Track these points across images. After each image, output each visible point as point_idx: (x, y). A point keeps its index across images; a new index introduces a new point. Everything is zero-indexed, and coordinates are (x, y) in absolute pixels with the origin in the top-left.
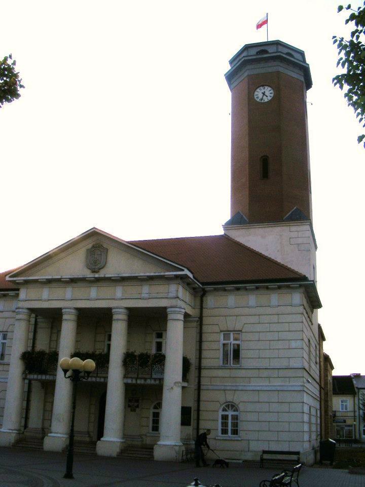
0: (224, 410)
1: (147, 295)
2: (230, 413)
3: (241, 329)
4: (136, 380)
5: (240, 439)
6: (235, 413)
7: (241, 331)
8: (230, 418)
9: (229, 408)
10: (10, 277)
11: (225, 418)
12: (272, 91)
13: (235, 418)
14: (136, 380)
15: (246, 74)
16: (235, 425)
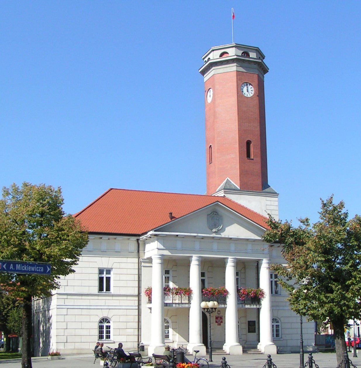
1: (251, 250)
2: (105, 325)
5: (282, 339)
6: (277, 324)
8: (105, 327)
9: (104, 321)
10: (155, 231)
11: (101, 327)
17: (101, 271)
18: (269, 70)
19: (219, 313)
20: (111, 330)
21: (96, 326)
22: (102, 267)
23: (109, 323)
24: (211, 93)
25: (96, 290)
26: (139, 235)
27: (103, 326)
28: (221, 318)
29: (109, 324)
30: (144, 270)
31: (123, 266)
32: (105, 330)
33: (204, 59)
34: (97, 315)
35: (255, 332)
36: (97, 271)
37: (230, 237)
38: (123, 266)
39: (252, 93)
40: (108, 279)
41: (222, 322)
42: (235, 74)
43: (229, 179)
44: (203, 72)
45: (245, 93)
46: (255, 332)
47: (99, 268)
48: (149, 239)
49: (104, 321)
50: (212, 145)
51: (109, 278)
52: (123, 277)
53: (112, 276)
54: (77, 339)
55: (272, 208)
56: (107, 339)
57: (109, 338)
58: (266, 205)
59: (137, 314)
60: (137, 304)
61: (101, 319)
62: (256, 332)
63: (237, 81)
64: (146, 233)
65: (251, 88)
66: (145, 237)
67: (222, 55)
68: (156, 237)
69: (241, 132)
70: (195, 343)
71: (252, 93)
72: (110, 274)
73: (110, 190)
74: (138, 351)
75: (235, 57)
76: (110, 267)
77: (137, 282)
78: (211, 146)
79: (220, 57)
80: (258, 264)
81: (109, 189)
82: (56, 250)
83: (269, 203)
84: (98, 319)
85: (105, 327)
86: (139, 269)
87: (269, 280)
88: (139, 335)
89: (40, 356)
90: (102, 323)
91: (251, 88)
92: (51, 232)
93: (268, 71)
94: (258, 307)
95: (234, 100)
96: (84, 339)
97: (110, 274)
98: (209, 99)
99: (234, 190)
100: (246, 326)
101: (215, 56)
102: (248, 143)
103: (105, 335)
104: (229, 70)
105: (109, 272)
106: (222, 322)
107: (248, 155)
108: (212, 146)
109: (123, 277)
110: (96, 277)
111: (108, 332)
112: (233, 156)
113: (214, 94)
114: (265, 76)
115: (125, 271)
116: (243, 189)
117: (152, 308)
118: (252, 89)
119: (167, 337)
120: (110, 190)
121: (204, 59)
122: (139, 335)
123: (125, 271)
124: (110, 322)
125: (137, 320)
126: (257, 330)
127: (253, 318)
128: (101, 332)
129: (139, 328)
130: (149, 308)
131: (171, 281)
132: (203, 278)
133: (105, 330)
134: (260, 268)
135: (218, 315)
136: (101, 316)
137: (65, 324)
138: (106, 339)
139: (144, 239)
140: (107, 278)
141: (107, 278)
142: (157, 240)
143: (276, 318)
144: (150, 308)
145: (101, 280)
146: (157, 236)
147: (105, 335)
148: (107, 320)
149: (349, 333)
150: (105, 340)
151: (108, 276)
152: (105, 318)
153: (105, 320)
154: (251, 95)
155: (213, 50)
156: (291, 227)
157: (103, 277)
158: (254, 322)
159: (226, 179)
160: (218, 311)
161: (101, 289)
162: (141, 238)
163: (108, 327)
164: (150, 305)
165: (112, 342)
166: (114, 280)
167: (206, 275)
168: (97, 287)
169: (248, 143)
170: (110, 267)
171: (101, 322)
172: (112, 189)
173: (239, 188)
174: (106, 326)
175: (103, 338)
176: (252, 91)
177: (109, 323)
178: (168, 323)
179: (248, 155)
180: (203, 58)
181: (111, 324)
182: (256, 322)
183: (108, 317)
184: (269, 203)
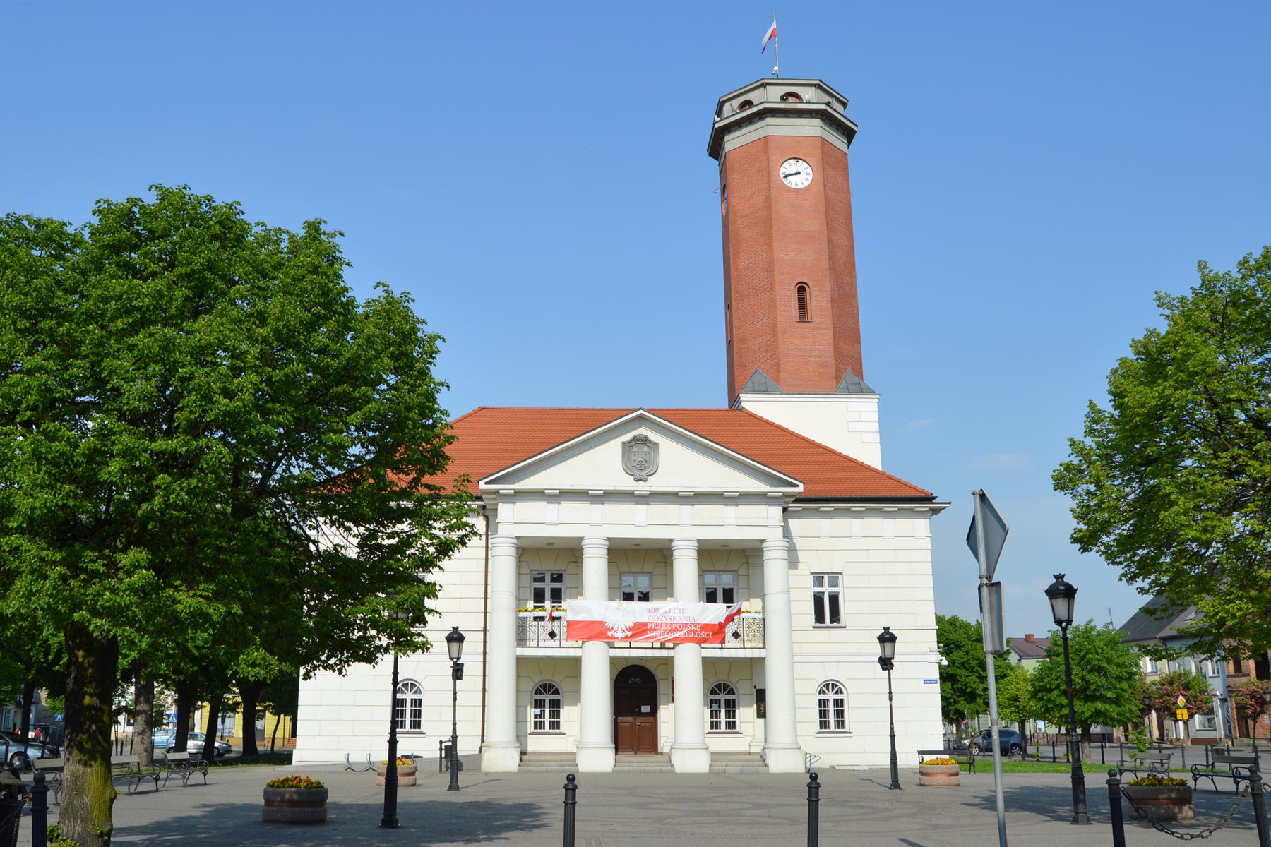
0: (821, 692)
2: (831, 696)
8: (831, 703)
9: (828, 689)
10: (486, 483)
11: (823, 703)
12: (810, 177)
13: (839, 703)
16: (840, 714)
32: (408, 709)
39: (807, 179)
49: (828, 689)
56: (552, 731)
67: (784, 98)
79: (717, 159)
82: (1240, 524)
85: (831, 703)
92: (28, 554)
103: (408, 719)
105: (834, 581)
132: (636, 597)
133: (408, 709)
136: (823, 679)
143: (842, 688)
145: (818, 600)
147: (408, 719)
148: (554, 686)
149: (116, 732)
151: (834, 590)
153: (830, 686)
156: (417, 489)
161: (819, 617)
174: (412, 700)
178: (841, 692)
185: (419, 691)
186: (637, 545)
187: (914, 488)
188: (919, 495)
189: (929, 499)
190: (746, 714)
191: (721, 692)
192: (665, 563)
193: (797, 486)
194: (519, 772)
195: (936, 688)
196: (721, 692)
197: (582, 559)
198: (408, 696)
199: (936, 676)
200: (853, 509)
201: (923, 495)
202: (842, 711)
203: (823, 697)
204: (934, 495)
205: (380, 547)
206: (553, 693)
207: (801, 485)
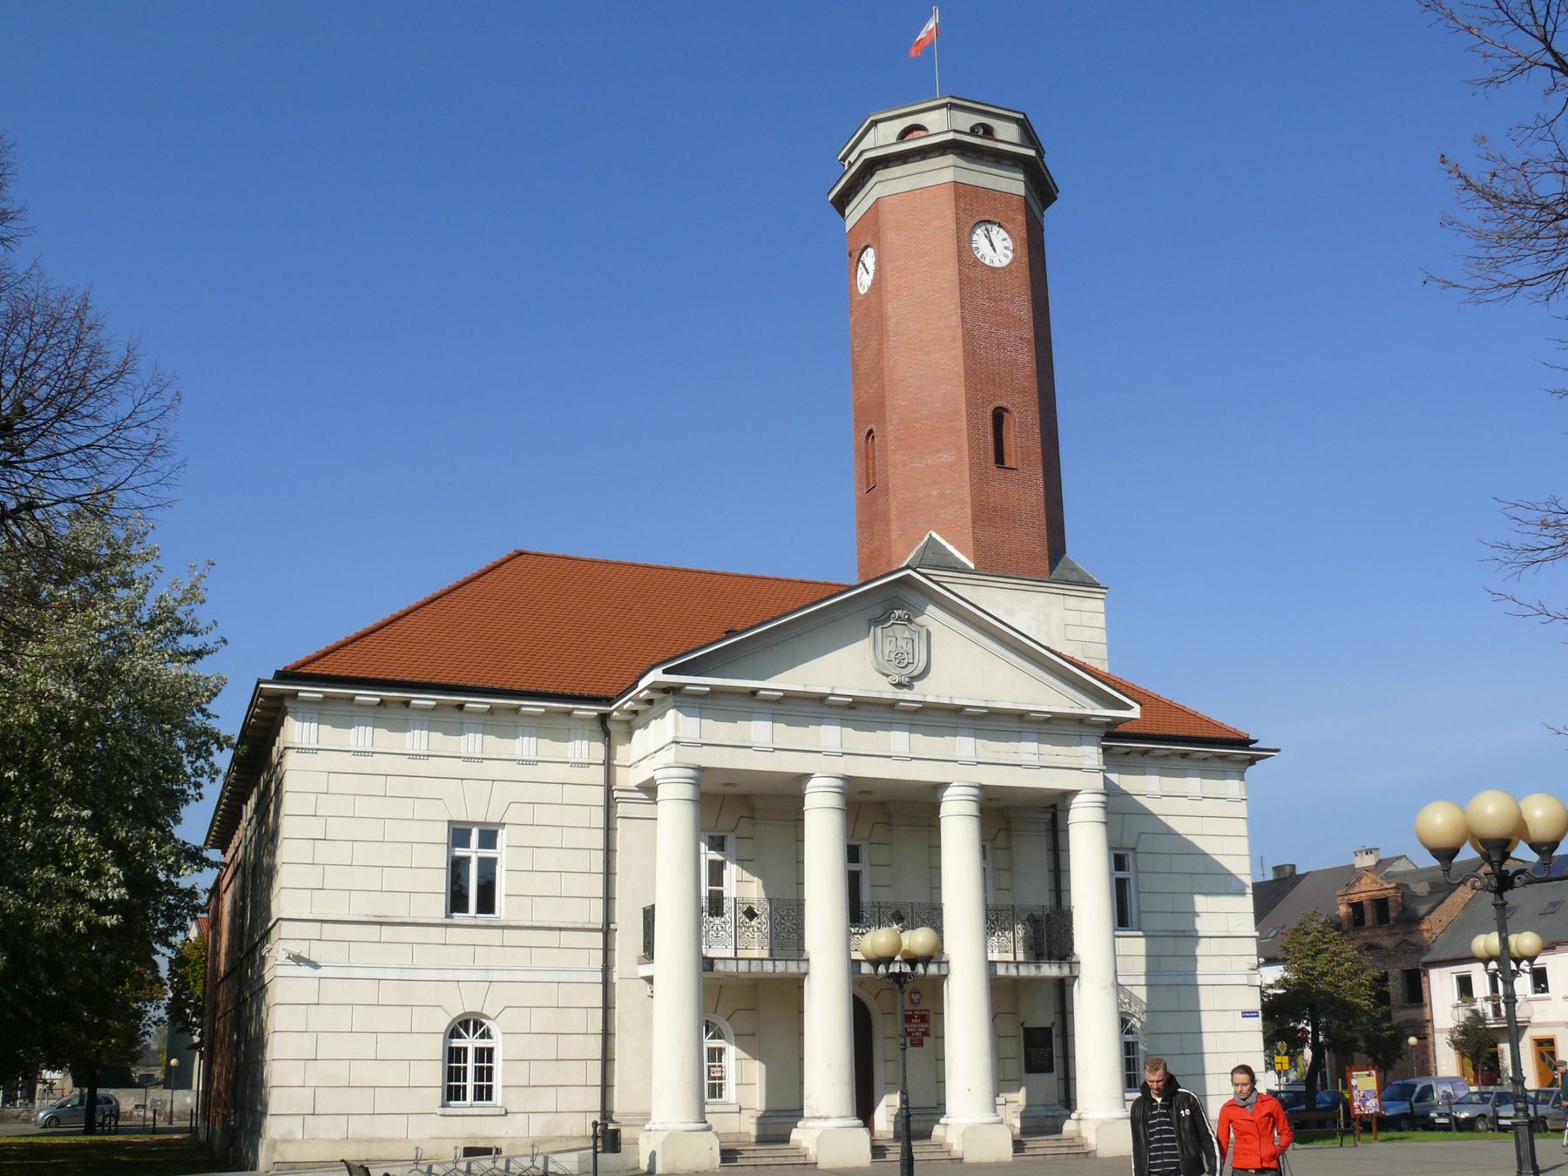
2: (471, 1043)
3: (1133, 847)
4: (1017, 968)
7: (1134, 849)
10: (665, 672)
11: (455, 1055)
14: (1017, 968)
15: (948, 176)
17: (459, 835)
18: (1058, 195)
19: (915, 997)
20: (498, 1065)
21: (435, 1048)
22: (464, 818)
23: (490, 1037)
24: (869, 258)
25: (437, 906)
26: (609, 701)
27: (465, 1049)
28: (924, 1019)
29: (486, 1040)
30: (624, 833)
31: (544, 815)
32: (471, 1065)
33: (844, 159)
34: (440, 1006)
35: (1052, 1071)
36: (442, 834)
37: (958, 702)
38: (544, 815)
39: (1006, 256)
40: (487, 867)
41: (926, 1034)
42: (948, 197)
43: (935, 535)
44: (842, 202)
45: (983, 255)
46: (1052, 1071)
47: (450, 822)
48: (645, 711)
50: (875, 429)
51: (493, 861)
52: (546, 860)
53: (502, 852)
54: (359, 1101)
55: (1087, 634)
57: (489, 1098)
58: (1066, 625)
59: (598, 1001)
60: (599, 964)
61: (456, 1023)
62: (1055, 1070)
63: (957, 214)
64: (635, 685)
65: (1005, 239)
66: (629, 700)
67: (904, 135)
68: (670, 698)
69: (976, 373)
70: (826, 1118)
71: (1006, 256)
72: (494, 847)
73: (513, 558)
74: (596, 1153)
75: (950, 136)
76: (493, 817)
77: (600, 879)
78: (871, 432)
80: (1054, 816)
81: (510, 551)
83: (1072, 617)
84: (443, 1023)
86: (609, 830)
87: (1111, 874)
88: (606, 1086)
89: (935, 955)
90: (460, 1036)
91: (1005, 239)
93: (1056, 199)
94: (1066, 971)
95: (948, 274)
96: (385, 1102)
97: (494, 847)
98: (864, 281)
99: (955, 569)
100: (1016, 1048)
101: (883, 138)
102: (999, 416)
103: (470, 1083)
104: (927, 181)
105: (488, 839)
106: (926, 1034)
107: (1000, 458)
108: (875, 433)
109: (546, 860)
110: (439, 858)
111: (484, 1074)
112: (947, 457)
113: (879, 263)
114: (1045, 213)
115: (551, 837)
116: (986, 569)
117: (655, 980)
118: (1005, 243)
119: (716, 1090)
120: (513, 558)
121: (844, 159)
122: (606, 1086)
123: (551, 837)
124: (493, 1033)
125: (599, 1027)
126: (1057, 1063)
127: (1043, 1017)
128: (454, 1074)
129: (607, 1060)
130: (644, 978)
131: (732, 862)
133: (471, 1065)
134: (1234, 732)
135: (912, 1008)
136: (457, 1011)
137: (308, 1039)
138: (475, 1100)
139: (626, 711)
140: (481, 861)
141: (481, 861)
142: (677, 707)
144: (650, 980)
145: (457, 868)
146: (674, 694)
147: (470, 1083)
150: (471, 1106)
152: (472, 1017)
154: (1006, 262)
155: (875, 123)
157: (467, 860)
158: (1047, 1032)
159: (928, 536)
160: (911, 993)
161: (457, 902)
162: (614, 707)
163: (485, 1055)
164: (645, 970)
165: (497, 1111)
166: (507, 870)
167: (863, 854)
168: (444, 896)
169: (999, 416)
170: (496, 820)
171: (454, 1033)
172: (521, 553)
173: (973, 568)
174: (476, 1049)
175: (464, 1099)
176: (1006, 248)
177: (490, 1037)
179: (1000, 458)
180: (839, 158)
181: (497, 1043)
182: (1054, 1032)
183: (467, 1011)
184: (1072, 617)
185: (486, 1035)
186: (731, 785)
187: (1220, 727)
188: (1224, 735)
189: (1245, 743)
190: (54, 1082)
191: (468, 1033)
192: (890, 825)
193: (1129, 708)
194: (1014, 1161)
195: (1257, 1023)
196: (468, 1033)
197: (939, 820)
198: (471, 1043)
199: (1256, 1005)
200: (357, 698)
201: (1237, 737)
202: (490, 1069)
203: (456, 1043)
204: (1252, 737)
205: (141, 752)
206: (482, 1036)
207: (1137, 707)
